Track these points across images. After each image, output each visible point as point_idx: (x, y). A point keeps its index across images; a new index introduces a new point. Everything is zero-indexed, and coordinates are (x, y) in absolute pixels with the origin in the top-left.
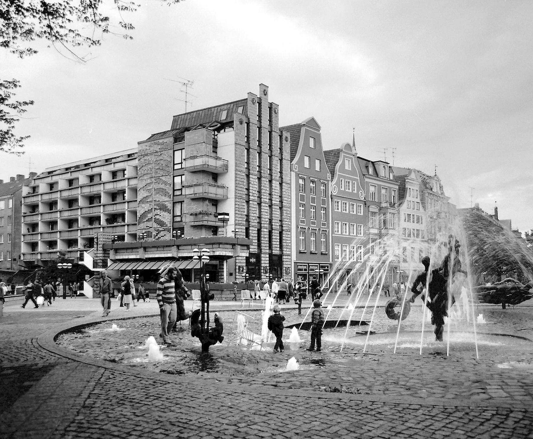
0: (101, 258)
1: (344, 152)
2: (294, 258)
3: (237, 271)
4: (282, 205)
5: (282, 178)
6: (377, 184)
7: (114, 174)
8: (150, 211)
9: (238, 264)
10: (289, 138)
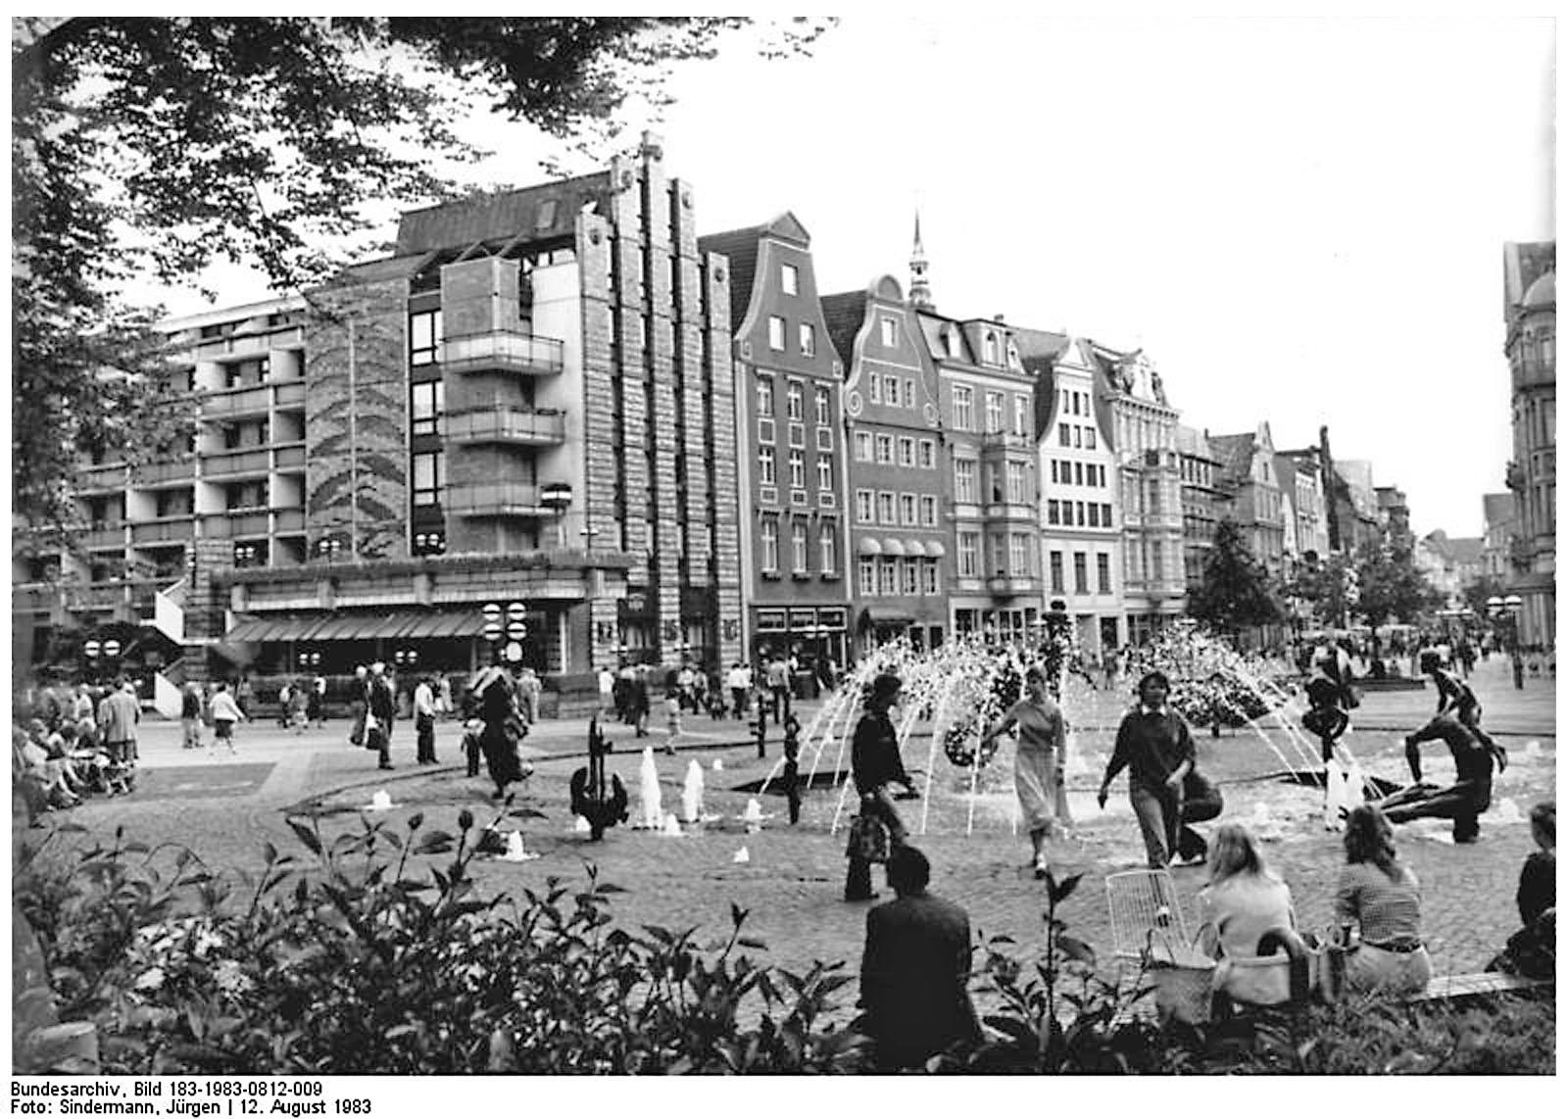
0: (205, 609)
1: (880, 301)
2: (748, 593)
3: (595, 635)
4: (712, 452)
5: (710, 382)
6: (975, 384)
7: (231, 369)
8: (343, 477)
9: (596, 618)
10: (726, 270)
